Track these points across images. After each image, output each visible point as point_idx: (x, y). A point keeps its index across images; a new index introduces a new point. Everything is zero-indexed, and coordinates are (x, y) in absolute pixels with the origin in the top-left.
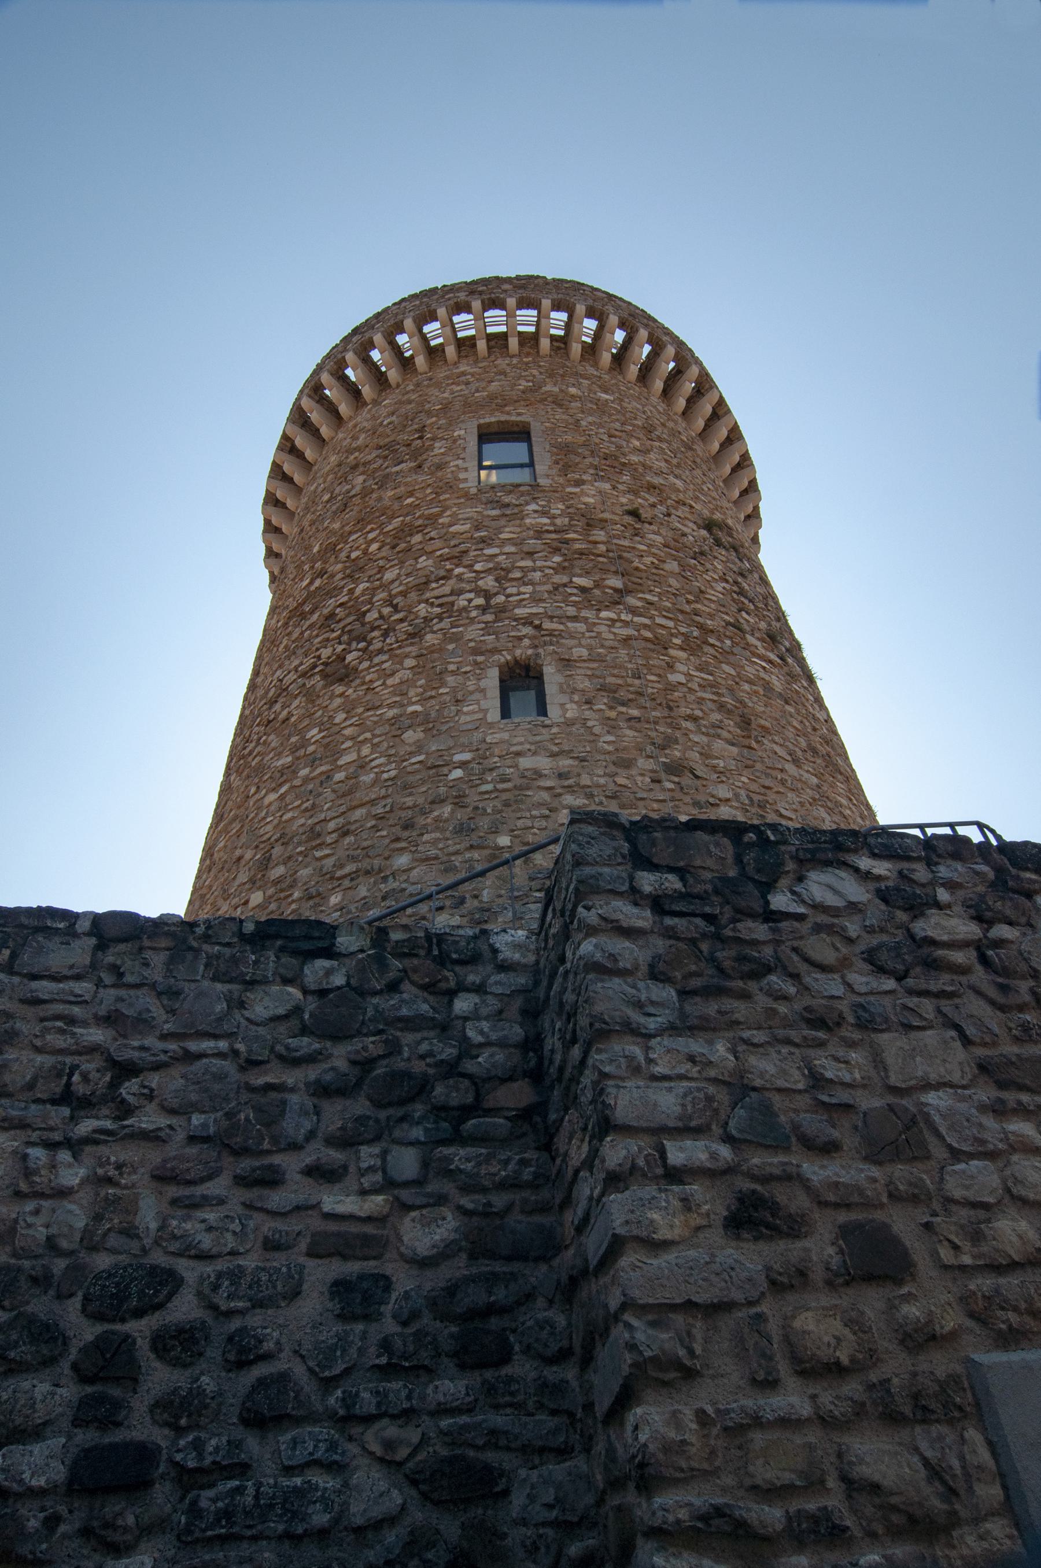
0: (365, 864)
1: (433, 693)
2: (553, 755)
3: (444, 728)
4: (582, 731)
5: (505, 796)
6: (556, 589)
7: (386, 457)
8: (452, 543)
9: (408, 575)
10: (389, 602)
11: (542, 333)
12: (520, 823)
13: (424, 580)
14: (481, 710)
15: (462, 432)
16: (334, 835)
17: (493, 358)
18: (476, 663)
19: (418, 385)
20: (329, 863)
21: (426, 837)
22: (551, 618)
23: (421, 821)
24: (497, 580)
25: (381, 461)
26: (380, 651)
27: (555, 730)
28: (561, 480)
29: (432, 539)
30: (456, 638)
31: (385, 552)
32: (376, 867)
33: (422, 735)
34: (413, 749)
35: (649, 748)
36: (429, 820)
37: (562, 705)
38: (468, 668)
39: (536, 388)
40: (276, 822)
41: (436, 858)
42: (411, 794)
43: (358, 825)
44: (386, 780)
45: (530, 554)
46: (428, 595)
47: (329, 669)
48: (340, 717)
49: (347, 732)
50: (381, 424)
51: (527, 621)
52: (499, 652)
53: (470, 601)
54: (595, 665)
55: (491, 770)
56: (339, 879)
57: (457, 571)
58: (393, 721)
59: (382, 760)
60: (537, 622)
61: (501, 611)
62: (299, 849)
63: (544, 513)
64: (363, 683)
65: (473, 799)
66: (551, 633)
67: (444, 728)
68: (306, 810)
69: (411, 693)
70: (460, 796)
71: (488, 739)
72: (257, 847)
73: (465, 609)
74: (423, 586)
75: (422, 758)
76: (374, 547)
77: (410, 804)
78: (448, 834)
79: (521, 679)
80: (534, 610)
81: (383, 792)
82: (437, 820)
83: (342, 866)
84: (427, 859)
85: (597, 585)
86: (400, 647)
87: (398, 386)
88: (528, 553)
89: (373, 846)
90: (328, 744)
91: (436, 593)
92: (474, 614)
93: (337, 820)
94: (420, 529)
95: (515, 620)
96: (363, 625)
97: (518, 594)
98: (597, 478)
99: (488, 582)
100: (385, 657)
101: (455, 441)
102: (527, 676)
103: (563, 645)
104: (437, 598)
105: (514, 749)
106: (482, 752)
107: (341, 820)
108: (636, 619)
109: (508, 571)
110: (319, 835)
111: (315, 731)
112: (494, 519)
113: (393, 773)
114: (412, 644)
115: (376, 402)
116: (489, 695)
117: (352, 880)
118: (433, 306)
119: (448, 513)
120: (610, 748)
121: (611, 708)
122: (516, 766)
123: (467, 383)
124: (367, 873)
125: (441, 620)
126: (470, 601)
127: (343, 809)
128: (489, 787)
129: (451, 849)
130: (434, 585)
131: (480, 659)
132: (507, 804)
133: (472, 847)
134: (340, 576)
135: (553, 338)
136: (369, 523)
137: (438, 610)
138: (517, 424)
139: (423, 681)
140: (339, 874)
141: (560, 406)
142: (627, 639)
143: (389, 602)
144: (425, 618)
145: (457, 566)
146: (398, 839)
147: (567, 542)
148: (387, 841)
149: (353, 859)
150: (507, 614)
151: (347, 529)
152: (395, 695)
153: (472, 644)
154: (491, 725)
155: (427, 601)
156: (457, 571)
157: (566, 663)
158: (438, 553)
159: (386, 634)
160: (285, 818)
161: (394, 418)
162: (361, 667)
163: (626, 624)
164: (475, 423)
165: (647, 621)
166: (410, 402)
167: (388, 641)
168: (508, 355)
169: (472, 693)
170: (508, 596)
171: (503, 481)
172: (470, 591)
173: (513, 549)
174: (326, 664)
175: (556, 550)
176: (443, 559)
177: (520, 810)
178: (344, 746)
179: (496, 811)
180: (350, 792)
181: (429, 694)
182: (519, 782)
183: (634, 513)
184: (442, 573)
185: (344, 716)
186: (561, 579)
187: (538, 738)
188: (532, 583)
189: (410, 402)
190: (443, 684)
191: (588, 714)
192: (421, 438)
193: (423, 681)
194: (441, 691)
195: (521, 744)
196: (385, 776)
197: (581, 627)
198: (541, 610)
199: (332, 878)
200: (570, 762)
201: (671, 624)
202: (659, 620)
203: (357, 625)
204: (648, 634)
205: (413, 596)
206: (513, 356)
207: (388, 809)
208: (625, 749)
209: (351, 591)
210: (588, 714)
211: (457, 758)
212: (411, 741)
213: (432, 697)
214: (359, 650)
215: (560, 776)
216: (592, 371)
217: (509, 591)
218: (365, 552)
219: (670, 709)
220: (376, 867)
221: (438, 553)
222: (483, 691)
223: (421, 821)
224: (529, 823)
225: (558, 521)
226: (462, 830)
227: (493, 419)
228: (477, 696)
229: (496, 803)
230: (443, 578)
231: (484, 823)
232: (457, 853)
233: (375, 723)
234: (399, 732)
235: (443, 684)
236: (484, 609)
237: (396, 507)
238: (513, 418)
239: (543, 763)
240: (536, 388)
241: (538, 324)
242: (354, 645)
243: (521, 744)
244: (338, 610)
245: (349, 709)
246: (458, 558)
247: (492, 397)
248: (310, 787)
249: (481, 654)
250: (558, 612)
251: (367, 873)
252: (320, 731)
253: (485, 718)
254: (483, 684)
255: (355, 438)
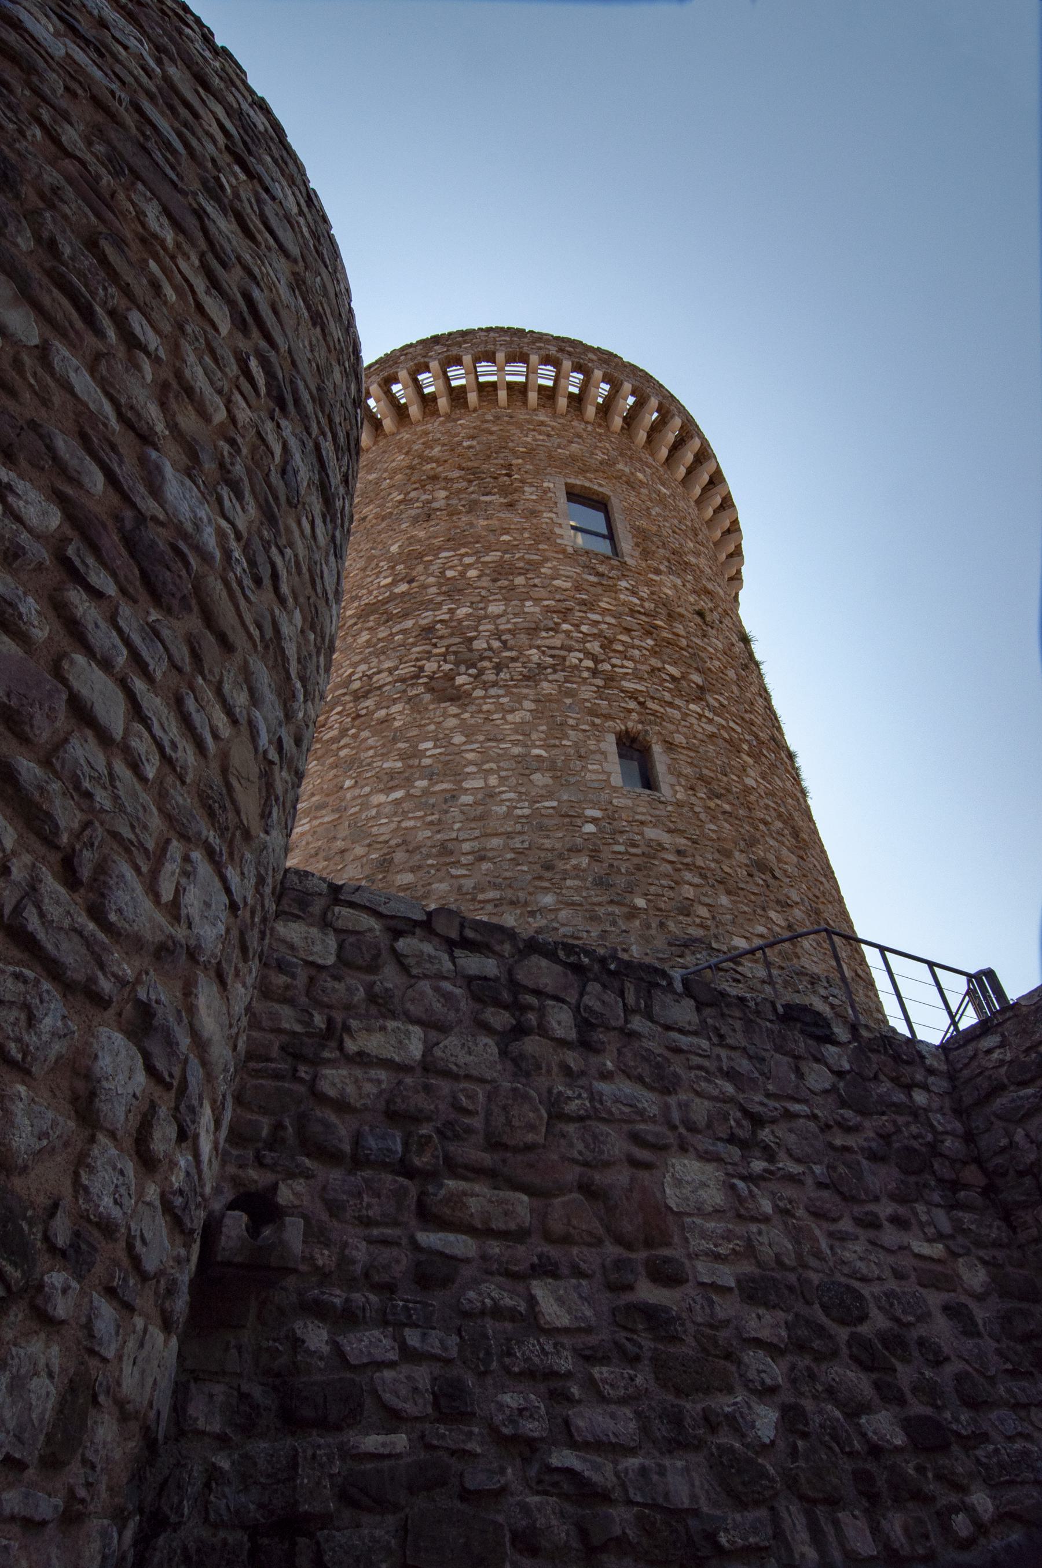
0: (509, 894)
1: (557, 742)
2: (670, 831)
3: (572, 780)
4: (690, 814)
5: (636, 860)
6: (653, 671)
7: (470, 481)
8: (558, 597)
9: (516, 615)
10: (498, 634)
11: (561, 391)
12: (652, 889)
13: (533, 626)
14: (604, 772)
15: (551, 485)
16: (470, 857)
17: (569, 417)
18: (593, 724)
19: (497, 417)
20: (468, 884)
21: (569, 882)
22: (653, 698)
23: (561, 865)
24: (601, 647)
25: (465, 484)
26: (495, 684)
27: (670, 808)
28: (644, 564)
29: (535, 586)
30: (571, 693)
31: (485, 582)
32: (522, 900)
33: (550, 781)
34: (543, 792)
35: (742, 843)
36: (568, 867)
37: (672, 785)
38: (587, 727)
39: (611, 463)
40: (393, 826)
41: (581, 905)
42: (548, 837)
43: (495, 853)
44: (519, 817)
45: (628, 630)
46: (539, 642)
47: (433, 684)
48: (458, 739)
49: (470, 756)
50: (460, 443)
51: (633, 695)
52: (613, 719)
53: (581, 660)
54: (692, 754)
55: (622, 832)
56: (480, 902)
57: (565, 627)
58: (519, 759)
59: (512, 795)
60: (642, 699)
61: (610, 679)
62: (430, 862)
63: (634, 593)
64: (480, 711)
65: (606, 854)
66: (654, 713)
67: (572, 780)
68: (431, 823)
69: (534, 736)
70: (595, 851)
71: (615, 802)
72: (369, 845)
73: (576, 667)
74: (533, 631)
75: (555, 804)
76: (472, 573)
77: (549, 846)
78: (588, 884)
79: (633, 748)
80: (638, 687)
81: (518, 827)
82: (576, 868)
83: (483, 891)
84: (573, 904)
85: (683, 678)
86: (515, 686)
87: (475, 410)
88: (625, 629)
89: (516, 879)
90: (447, 763)
91: (547, 642)
92: (585, 674)
93: (472, 844)
94: (523, 572)
95: (623, 691)
96: (471, 650)
97: (622, 667)
98: (671, 571)
99: (594, 647)
100: (501, 692)
101: (545, 492)
102: (631, 747)
103: (665, 728)
104: (549, 648)
105: (638, 817)
106: (611, 815)
107: (475, 844)
108: (716, 718)
109: (611, 642)
110: (452, 853)
111: (430, 744)
112: (593, 585)
113: (527, 812)
114: (527, 686)
115: (448, 416)
116: (610, 758)
117: (496, 906)
118: (526, 349)
119: (549, 565)
120: (714, 836)
121: (710, 798)
122: (642, 834)
123: (549, 435)
124: (512, 903)
125: (555, 671)
126: (581, 660)
127: (477, 833)
128: (622, 848)
129: (595, 900)
130: (544, 634)
131: (597, 721)
132: (638, 868)
133: (612, 902)
134: (433, 590)
135: (571, 395)
136: (464, 545)
137: (549, 660)
138: (598, 493)
139: (544, 728)
140: (481, 897)
141: (633, 488)
142: (712, 736)
143: (498, 634)
144: (539, 664)
145: (564, 621)
146: (540, 878)
147: (656, 627)
148: (529, 877)
149: (496, 886)
150: (614, 684)
151: (437, 542)
152: (517, 733)
153: (588, 705)
154: (615, 789)
155: (538, 647)
156: (565, 627)
157: (670, 746)
158: (546, 603)
159: (498, 668)
160: (404, 825)
161: (474, 443)
162: (475, 694)
163: (710, 721)
164: (563, 481)
165: (724, 722)
166: (491, 433)
167: (502, 675)
168: (583, 420)
169: (593, 752)
170: (614, 666)
171: (589, 547)
172: (579, 651)
173: (613, 621)
174: (431, 678)
175: (649, 633)
176: (548, 610)
177: (649, 876)
178: (467, 770)
179: (629, 873)
180: (481, 818)
181: (553, 742)
182: (647, 850)
183: (700, 614)
184: (551, 625)
185: (464, 739)
186: (655, 662)
187: (658, 812)
188: (631, 659)
189: (491, 433)
190: (566, 736)
191: (693, 799)
192: (509, 475)
193: (544, 728)
194: (564, 742)
195: (643, 814)
196: (519, 812)
197: (677, 715)
198: (644, 689)
199: (474, 900)
200: (683, 841)
201: (739, 729)
202: (732, 724)
203: (462, 648)
204: (726, 736)
205: (523, 638)
206: (587, 423)
207: (526, 845)
208: (725, 839)
209: (451, 611)
210: (693, 799)
211: (589, 813)
212: (540, 784)
213: (555, 746)
214: (470, 675)
215: (679, 852)
216: (650, 460)
217: (614, 661)
218: (463, 574)
219: (750, 809)
220: (522, 900)
221: (546, 603)
222: (603, 753)
223: (561, 865)
224: (660, 891)
225: (646, 604)
226: (601, 883)
227: (578, 482)
228: (598, 757)
229: (628, 864)
230: (551, 629)
231: (621, 881)
232: (600, 904)
233: (499, 755)
234: (527, 772)
235: (566, 736)
236: (595, 673)
237: (492, 538)
238: (596, 487)
239: (665, 838)
240: (611, 463)
241: (556, 381)
242: (463, 669)
243: (643, 814)
244: (438, 626)
245: (470, 733)
246: (565, 614)
247: (573, 458)
248: (432, 801)
249: (597, 716)
250: (657, 695)
251: (512, 903)
252: (435, 747)
253: (608, 781)
254: (603, 746)
255: (428, 445)
